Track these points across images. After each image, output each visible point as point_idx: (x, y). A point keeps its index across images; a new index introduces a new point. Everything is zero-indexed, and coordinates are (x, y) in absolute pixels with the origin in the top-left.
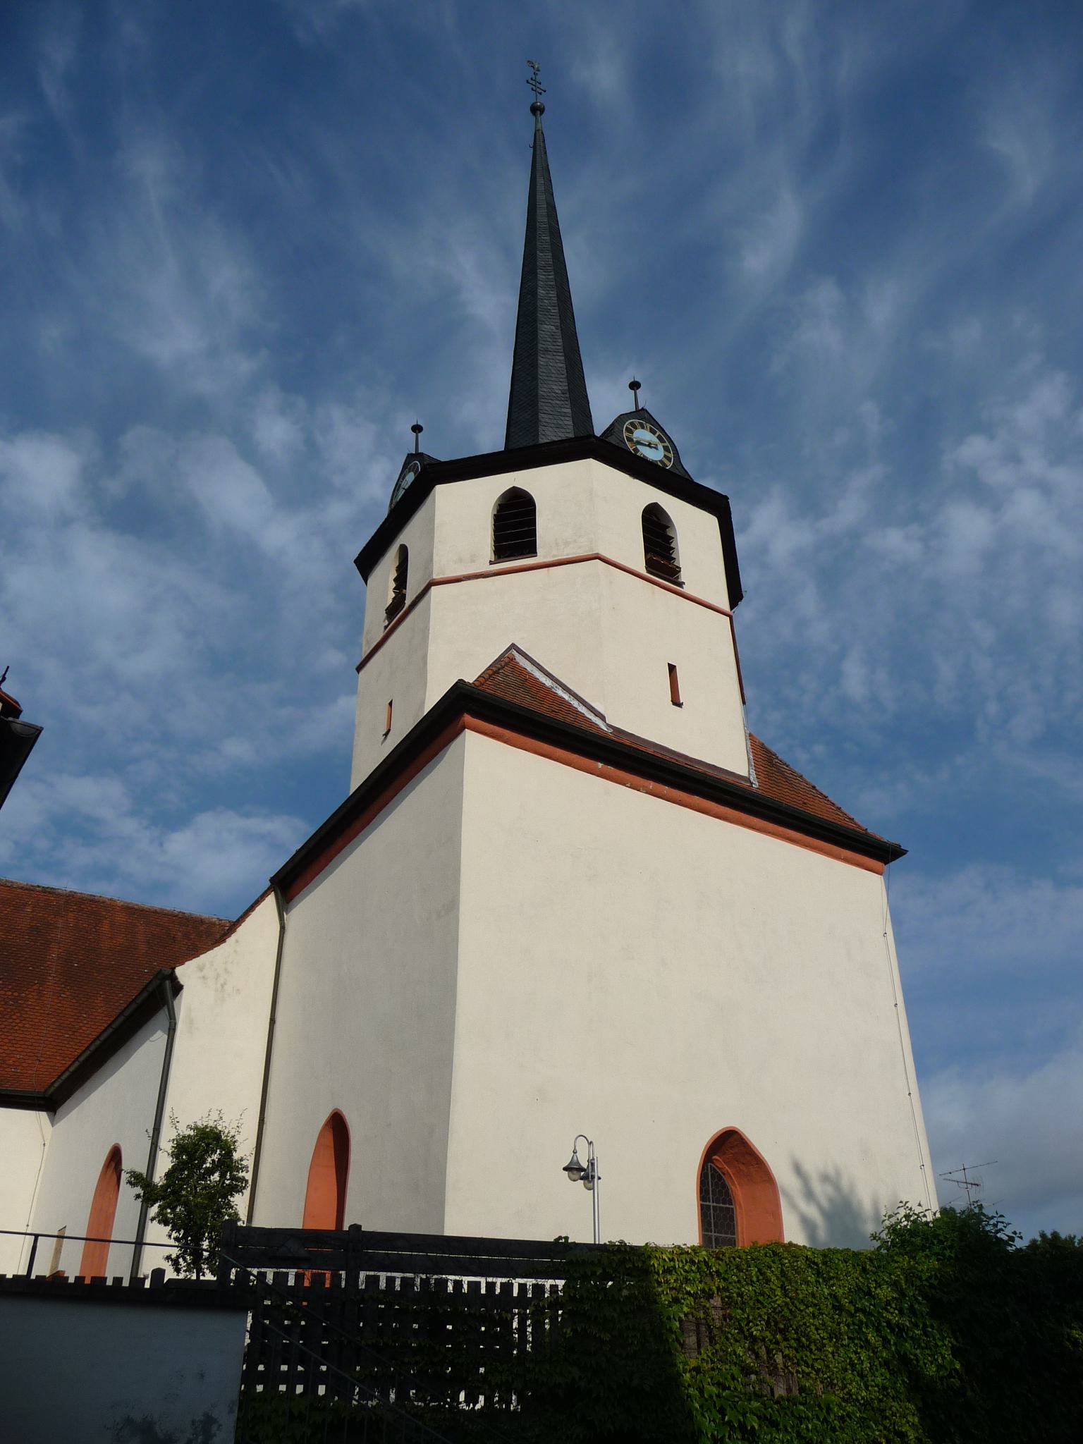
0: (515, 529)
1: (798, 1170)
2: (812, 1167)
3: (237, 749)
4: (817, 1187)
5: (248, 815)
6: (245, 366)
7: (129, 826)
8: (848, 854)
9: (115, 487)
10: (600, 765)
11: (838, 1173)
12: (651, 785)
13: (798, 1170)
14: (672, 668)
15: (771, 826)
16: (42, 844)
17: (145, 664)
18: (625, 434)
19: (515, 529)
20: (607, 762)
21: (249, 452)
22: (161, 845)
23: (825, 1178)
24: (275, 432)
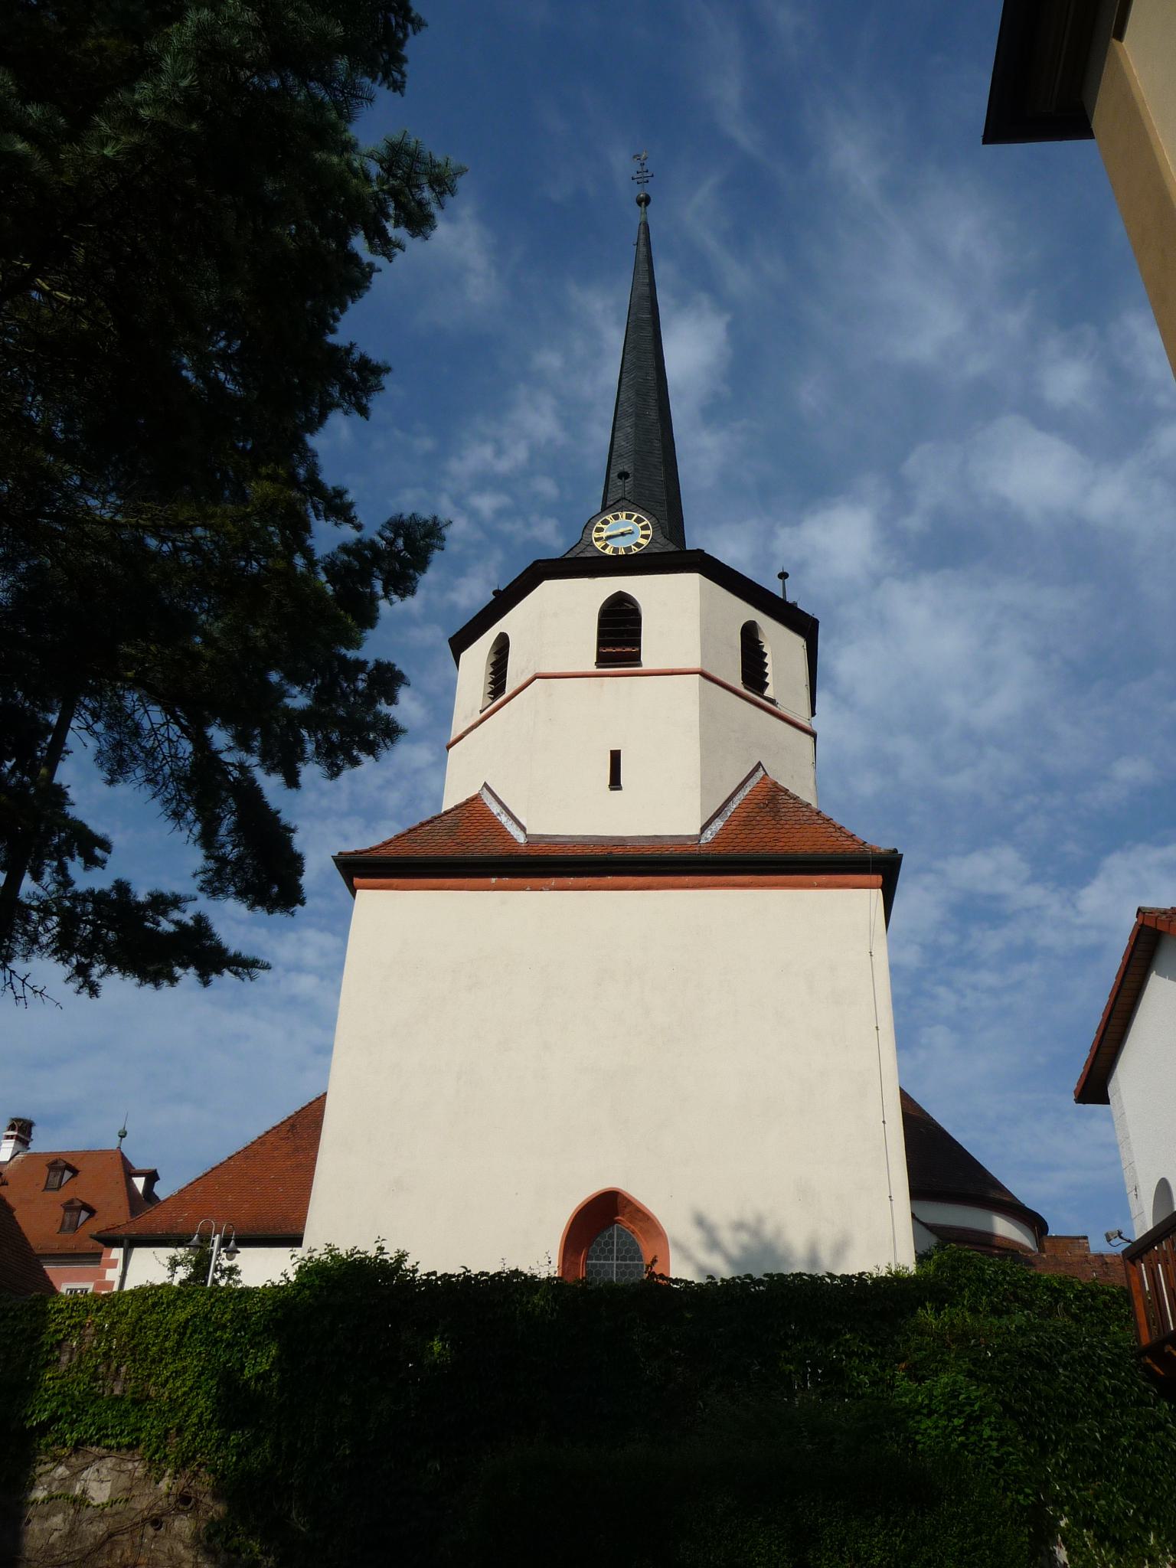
0: (619, 635)
1: (701, 1222)
2: (721, 1215)
3: (1132, 770)
4: (726, 1237)
5: (1163, 843)
6: (1014, 322)
7: (1034, 894)
8: (824, 878)
9: (914, 523)
10: (493, 880)
11: (760, 1220)
12: (553, 881)
13: (701, 1222)
14: (615, 756)
15: (709, 879)
16: (949, 939)
17: (1003, 704)
18: (646, 522)
19: (619, 635)
20: (500, 875)
21: (1045, 418)
22: (1074, 906)
23: (739, 1226)
24: (1068, 381)
